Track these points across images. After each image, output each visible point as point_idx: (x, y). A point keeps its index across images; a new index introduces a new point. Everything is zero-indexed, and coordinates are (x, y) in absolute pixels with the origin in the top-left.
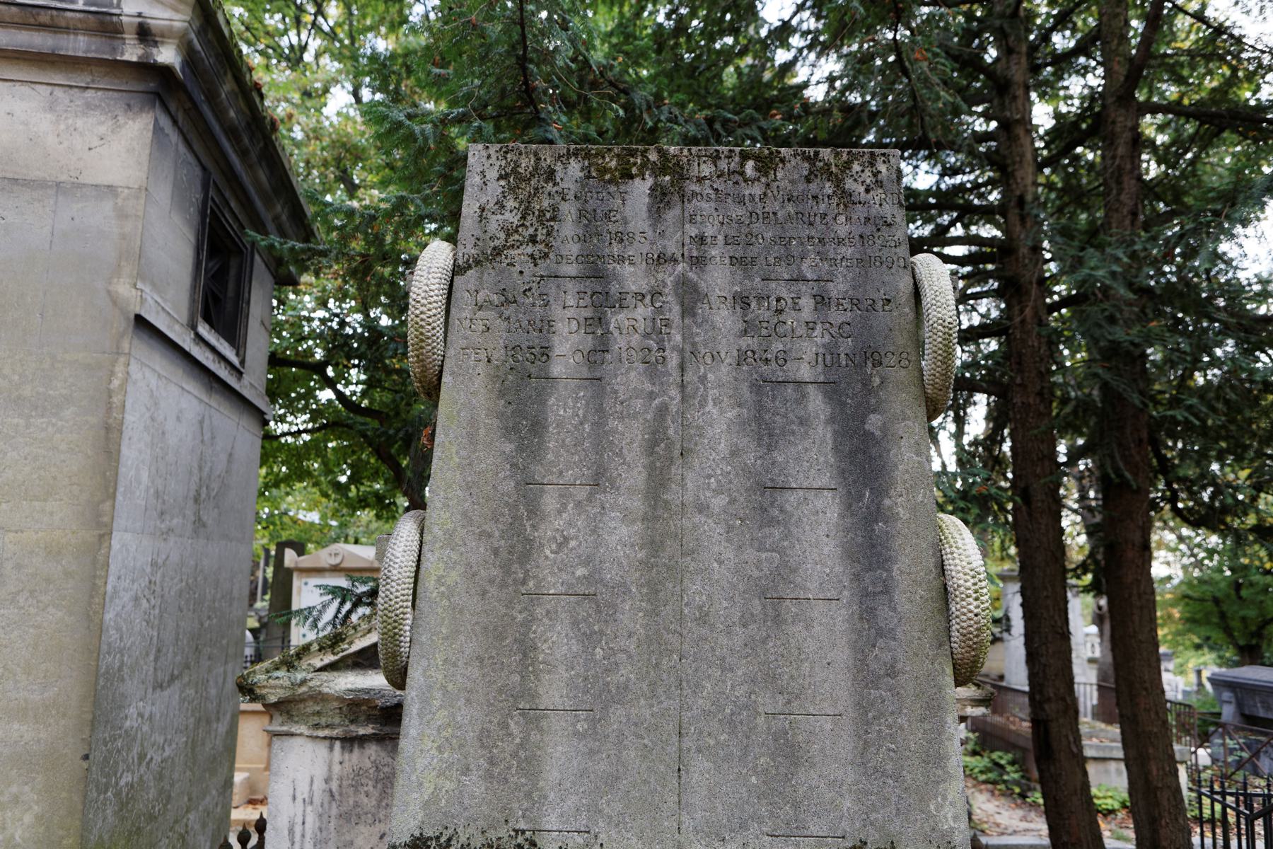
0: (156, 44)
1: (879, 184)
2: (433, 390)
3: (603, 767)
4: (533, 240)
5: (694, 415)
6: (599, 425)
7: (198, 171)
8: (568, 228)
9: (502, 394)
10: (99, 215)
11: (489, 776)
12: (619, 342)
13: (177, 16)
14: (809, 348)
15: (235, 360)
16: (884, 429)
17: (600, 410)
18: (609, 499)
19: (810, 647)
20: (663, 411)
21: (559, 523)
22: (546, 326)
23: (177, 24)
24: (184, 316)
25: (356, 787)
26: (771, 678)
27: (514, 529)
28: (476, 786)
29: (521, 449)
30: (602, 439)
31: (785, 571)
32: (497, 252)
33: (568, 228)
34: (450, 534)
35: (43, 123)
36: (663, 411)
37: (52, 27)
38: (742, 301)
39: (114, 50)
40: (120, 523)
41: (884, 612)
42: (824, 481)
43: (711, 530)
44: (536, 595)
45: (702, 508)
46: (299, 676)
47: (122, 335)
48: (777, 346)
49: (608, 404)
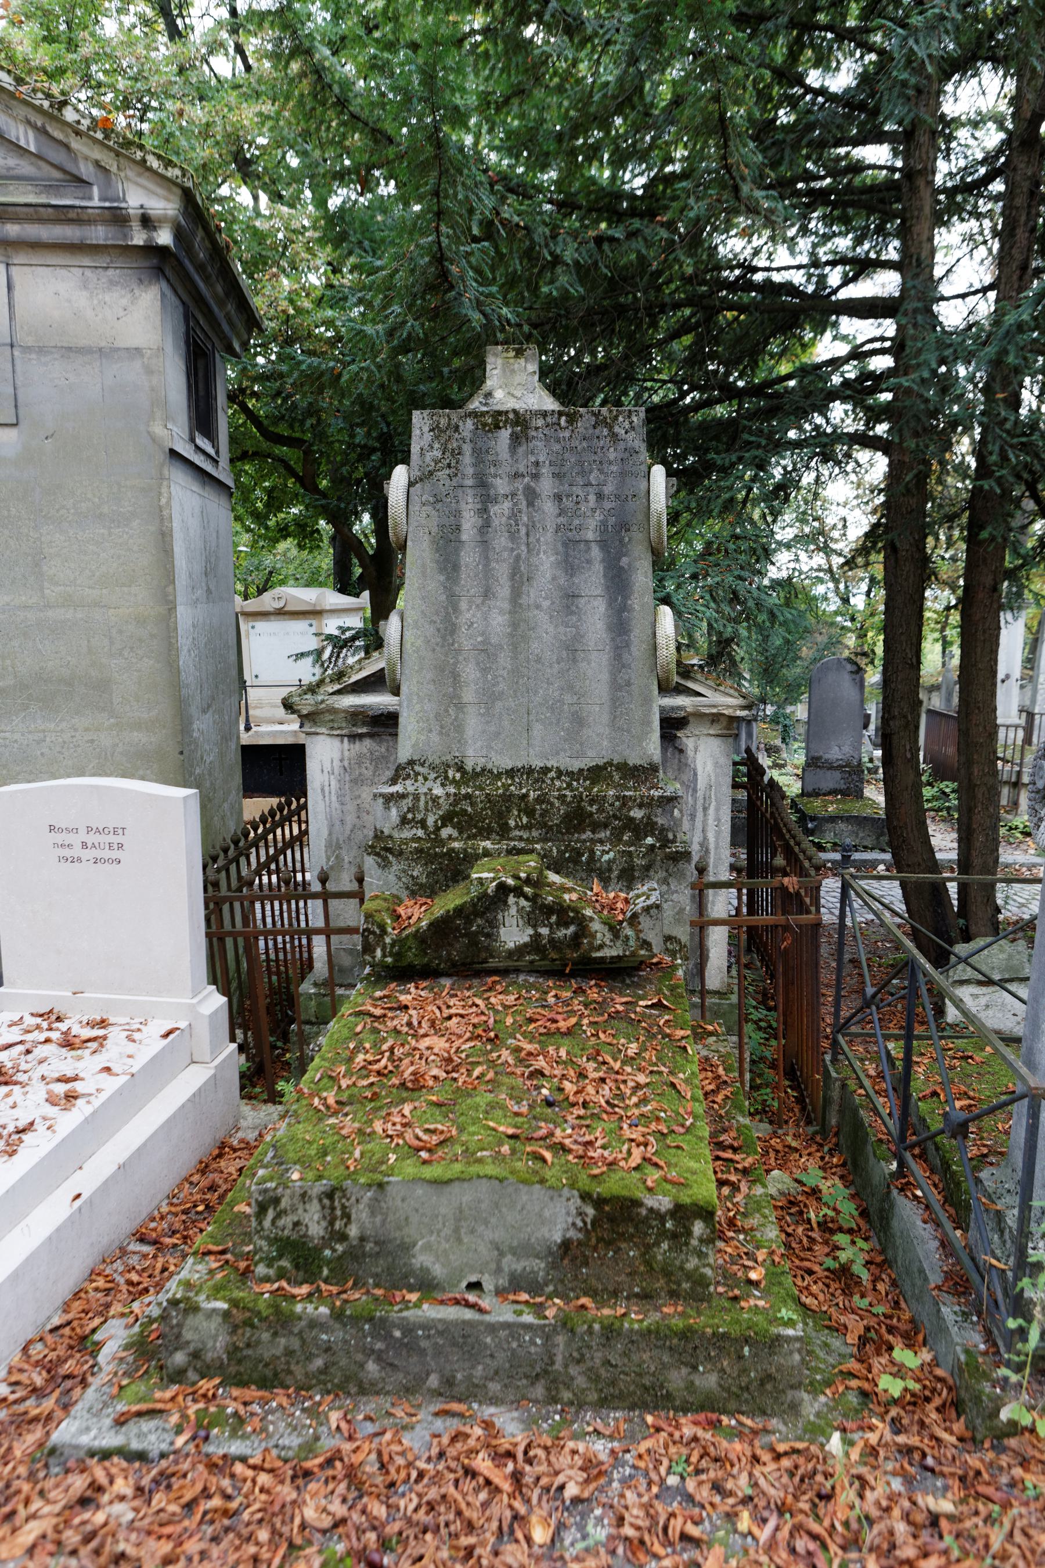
0: (155, 229)
1: (633, 428)
2: (403, 547)
3: (493, 729)
4: (449, 466)
5: (534, 560)
6: (487, 565)
7: (178, 302)
8: (467, 459)
9: (437, 550)
10: (132, 372)
11: (441, 733)
12: (496, 522)
13: (170, 206)
14: (592, 523)
15: (211, 451)
16: (629, 564)
17: (487, 558)
18: (492, 603)
19: (590, 673)
20: (518, 558)
21: (468, 616)
22: (457, 514)
23: (171, 212)
24: (186, 436)
25: (359, 764)
26: (570, 688)
27: (447, 618)
28: (435, 737)
29: (448, 579)
30: (488, 572)
31: (578, 637)
32: (431, 473)
33: (467, 459)
34: (416, 622)
35: (81, 300)
36: (518, 558)
37: (78, 221)
38: (558, 497)
39: (125, 237)
40: (179, 600)
41: (626, 656)
42: (598, 592)
43: (542, 617)
44: (459, 651)
45: (538, 607)
46: (320, 698)
47: (162, 465)
48: (576, 522)
49: (491, 554)
